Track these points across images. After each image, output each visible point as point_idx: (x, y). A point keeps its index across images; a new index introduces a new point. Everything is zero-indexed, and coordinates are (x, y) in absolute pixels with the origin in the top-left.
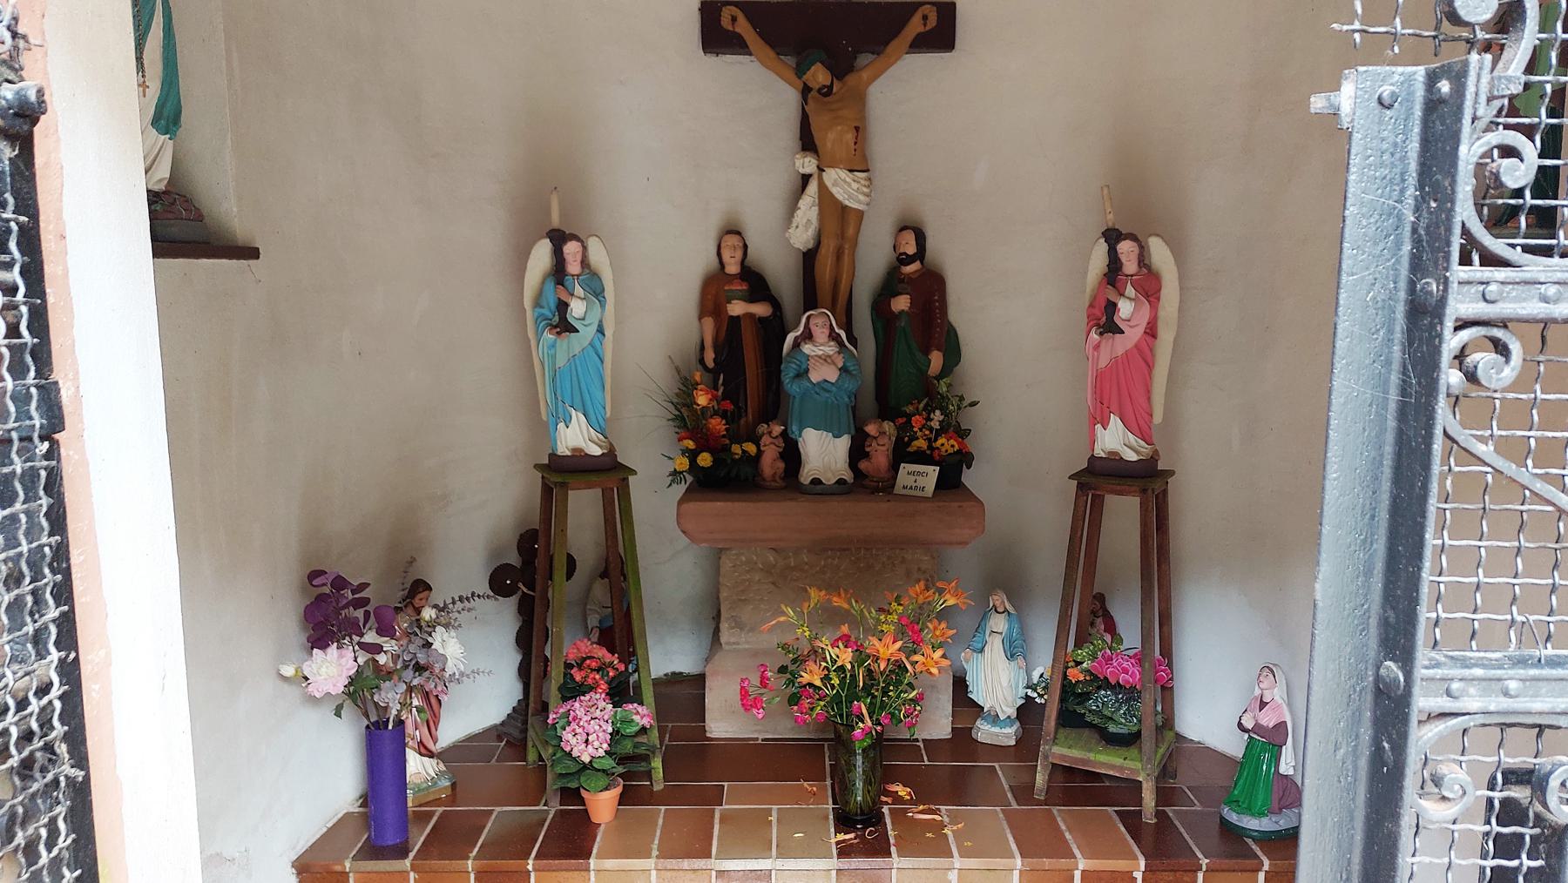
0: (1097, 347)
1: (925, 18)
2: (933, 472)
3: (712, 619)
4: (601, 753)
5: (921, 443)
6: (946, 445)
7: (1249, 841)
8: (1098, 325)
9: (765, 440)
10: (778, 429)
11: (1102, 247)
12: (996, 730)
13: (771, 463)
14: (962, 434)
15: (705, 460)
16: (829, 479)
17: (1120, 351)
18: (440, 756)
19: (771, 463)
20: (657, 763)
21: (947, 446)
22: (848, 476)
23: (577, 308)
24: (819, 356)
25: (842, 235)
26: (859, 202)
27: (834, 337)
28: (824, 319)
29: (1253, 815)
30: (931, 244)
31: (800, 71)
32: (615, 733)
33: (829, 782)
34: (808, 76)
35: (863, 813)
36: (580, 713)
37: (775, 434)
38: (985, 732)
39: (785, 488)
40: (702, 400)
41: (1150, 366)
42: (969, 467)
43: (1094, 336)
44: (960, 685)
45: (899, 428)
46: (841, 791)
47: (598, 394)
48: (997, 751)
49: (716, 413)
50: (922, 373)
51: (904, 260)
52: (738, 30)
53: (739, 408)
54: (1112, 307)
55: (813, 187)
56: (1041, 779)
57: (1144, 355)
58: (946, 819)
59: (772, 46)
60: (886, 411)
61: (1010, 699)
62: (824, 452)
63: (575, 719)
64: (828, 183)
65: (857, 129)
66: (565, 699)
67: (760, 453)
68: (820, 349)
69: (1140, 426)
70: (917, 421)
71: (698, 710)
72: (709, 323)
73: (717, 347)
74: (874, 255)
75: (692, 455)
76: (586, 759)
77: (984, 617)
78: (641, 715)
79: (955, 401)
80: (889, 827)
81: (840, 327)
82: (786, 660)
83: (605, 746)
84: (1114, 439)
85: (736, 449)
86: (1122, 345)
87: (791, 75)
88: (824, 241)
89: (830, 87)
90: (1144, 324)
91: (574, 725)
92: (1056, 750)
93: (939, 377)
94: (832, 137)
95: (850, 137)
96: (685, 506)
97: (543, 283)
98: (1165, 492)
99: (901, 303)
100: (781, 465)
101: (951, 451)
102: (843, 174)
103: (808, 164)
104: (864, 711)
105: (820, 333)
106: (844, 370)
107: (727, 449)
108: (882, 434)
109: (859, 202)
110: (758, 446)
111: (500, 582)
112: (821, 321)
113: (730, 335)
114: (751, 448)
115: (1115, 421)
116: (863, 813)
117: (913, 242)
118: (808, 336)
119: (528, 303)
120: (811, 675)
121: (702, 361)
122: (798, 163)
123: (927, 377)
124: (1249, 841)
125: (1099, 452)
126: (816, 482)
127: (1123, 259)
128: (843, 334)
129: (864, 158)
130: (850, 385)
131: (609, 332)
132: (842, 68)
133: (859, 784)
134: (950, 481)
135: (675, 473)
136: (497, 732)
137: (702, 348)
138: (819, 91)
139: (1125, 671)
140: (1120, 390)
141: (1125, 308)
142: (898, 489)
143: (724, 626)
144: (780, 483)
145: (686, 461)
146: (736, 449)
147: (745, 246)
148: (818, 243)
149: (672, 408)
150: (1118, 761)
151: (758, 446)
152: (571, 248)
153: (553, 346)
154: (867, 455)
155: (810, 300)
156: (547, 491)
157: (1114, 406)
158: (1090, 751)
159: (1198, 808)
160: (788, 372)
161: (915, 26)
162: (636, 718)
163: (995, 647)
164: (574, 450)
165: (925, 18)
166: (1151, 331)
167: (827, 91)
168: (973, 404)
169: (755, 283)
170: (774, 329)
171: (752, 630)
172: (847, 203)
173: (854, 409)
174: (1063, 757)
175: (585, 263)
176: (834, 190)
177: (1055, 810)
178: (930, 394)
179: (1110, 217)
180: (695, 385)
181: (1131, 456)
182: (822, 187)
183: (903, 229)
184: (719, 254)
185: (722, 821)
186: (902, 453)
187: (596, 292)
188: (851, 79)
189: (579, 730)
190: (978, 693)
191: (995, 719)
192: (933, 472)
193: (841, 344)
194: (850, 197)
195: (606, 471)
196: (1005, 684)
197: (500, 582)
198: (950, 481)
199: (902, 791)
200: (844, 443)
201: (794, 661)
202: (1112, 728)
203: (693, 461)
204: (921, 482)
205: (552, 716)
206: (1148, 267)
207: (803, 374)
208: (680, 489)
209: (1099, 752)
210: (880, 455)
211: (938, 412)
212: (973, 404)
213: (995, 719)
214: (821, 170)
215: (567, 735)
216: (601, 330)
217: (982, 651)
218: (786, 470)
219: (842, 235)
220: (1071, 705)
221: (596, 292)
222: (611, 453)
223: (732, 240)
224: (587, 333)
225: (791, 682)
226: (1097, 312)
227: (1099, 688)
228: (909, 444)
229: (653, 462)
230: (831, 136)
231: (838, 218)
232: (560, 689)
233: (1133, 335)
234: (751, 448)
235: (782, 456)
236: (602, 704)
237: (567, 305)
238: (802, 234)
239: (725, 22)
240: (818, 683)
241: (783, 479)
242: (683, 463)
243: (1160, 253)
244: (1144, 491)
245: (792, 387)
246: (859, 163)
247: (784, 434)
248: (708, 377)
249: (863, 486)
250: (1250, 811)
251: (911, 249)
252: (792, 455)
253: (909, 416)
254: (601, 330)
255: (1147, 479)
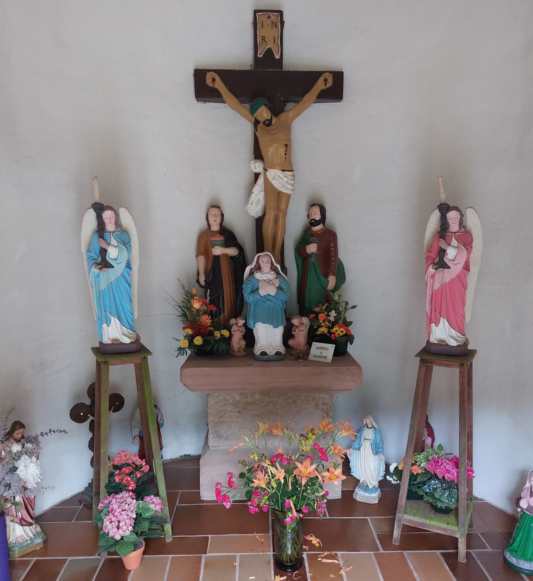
0: (433, 276)
1: (326, 80)
2: (331, 348)
3: (205, 423)
4: (128, 533)
5: (323, 330)
6: (338, 331)
7: (524, 576)
8: (434, 263)
9: (234, 328)
10: (241, 322)
11: (436, 215)
12: (367, 494)
13: (238, 341)
14: (347, 324)
15: (198, 341)
16: (271, 352)
17: (447, 280)
18: (38, 520)
19: (238, 341)
20: (168, 527)
21: (339, 332)
22: (282, 350)
23: (112, 253)
24: (266, 281)
25: (278, 208)
26: (288, 189)
27: (273, 268)
28: (268, 258)
29: (526, 560)
30: (328, 214)
31: (253, 111)
32: (139, 515)
33: (271, 534)
34: (257, 114)
35: (291, 561)
36: (115, 506)
37: (240, 325)
38: (360, 495)
39: (246, 355)
40: (197, 305)
41: (465, 287)
42: (351, 344)
43: (431, 270)
44: (346, 462)
45: (311, 320)
46: (278, 545)
47: (127, 306)
48: (367, 507)
49: (205, 313)
50: (325, 289)
51: (313, 223)
52: (216, 86)
53: (220, 309)
54: (442, 252)
55: (261, 180)
56: (397, 533)
57: (461, 281)
58: (341, 562)
59: (237, 96)
60: (303, 312)
61: (375, 476)
62: (268, 337)
63: (112, 510)
64: (270, 178)
65: (286, 145)
66: (109, 494)
67: (231, 336)
68: (265, 275)
69: (458, 325)
70: (322, 317)
71: (195, 481)
72: (202, 259)
73: (206, 273)
74: (295, 222)
75: (191, 338)
76: (118, 537)
77: (359, 430)
78: (155, 505)
79: (343, 305)
80: (307, 569)
81: (277, 263)
82: (245, 470)
83: (131, 528)
84: (443, 333)
85: (217, 334)
86: (448, 275)
87: (248, 113)
88: (268, 212)
89: (271, 120)
90: (464, 263)
91: (110, 515)
92: (406, 517)
93: (334, 291)
94: (272, 151)
95: (282, 150)
96: (185, 370)
97: (92, 237)
98: (471, 364)
99: (312, 248)
100: (243, 343)
101: (341, 334)
102: (278, 172)
103: (258, 167)
104: (292, 506)
105: (266, 266)
106: (279, 288)
107: (211, 334)
108: (303, 324)
109: (288, 189)
110: (230, 332)
111: (78, 414)
112: (266, 259)
113: (214, 265)
114: (226, 333)
115: (443, 322)
116: (291, 561)
117: (319, 213)
118: (258, 268)
119: (84, 250)
120: (260, 481)
121: (198, 281)
122: (252, 166)
123: (327, 290)
124: (524, 576)
125: (433, 340)
126: (264, 353)
127: (450, 222)
128: (279, 267)
129: (290, 163)
130: (283, 297)
131: (135, 267)
132: (277, 110)
133: (289, 546)
134: (341, 352)
135: (180, 349)
136: (78, 499)
137: (198, 274)
138: (264, 123)
139: (448, 471)
140: (447, 303)
141: (451, 253)
142: (311, 357)
143: (210, 436)
144: (243, 353)
145: (187, 342)
146: (217, 334)
147: (222, 215)
148: (264, 214)
149: (180, 310)
150: (444, 525)
151: (230, 332)
152: (107, 215)
153: (98, 276)
154: (293, 336)
155: (260, 247)
156: (98, 364)
157: (444, 312)
158: (426, 518)
159: (489, 550)
160: (247, 289)
161: (320, 86)
162: (152, 506)
163: (367, 448)
164: (113, 340)
165: (326, 80)
166: (467, 268)
167: (268, 123)
168: (354, 307)
169: (228, 237)
170: (239, 263)
171: (227, 438)
172: (280, 189)
173: (285, 310)
174: (409, 521)
175: (118, 224)
176: (274, 182)
177: (406, 552)
178: (329, 301)
179: (443, 196)
180: (193, 296)
181: (453, 343)
182: (266, 180)
183: (313, 205)
184: (207, 219)
185: (207, 565)
186: (313, 336)
187: (125, 242)
188: (283, 116)
189: (114, 519)
190: (356, 473)
191: (366, 488)
192: (331, 348)
193: (278, 273)
194: (283, 186)
195: (136, 352)
196: (372, 469)
197: (78, 414)
198: (341, 352)
199: (315, 541)
200: (279, 331)
201: (249, 471)
202: (439, 505)
203: (191, 342)
204: (324, 353)
205: (100, 505)
206: (464, 227)
207: (255, 291)
208: (184, 358)
209: (431, 519)
210: (300, 337)
211: (333, 311)
212: (354, 307)
213: (366, 488)
214: (265, 170)
215: (107, 523)
216: (129, 266)
217: (359, 449)
218: (247, 345)
219: (278, 208)
220: (414, 489)
221: (125, 242)
222: (137, 340)
223: (215, 211)
224: (119, 268)
225: (247, 484)
226: (433, 255)
227: (430, 479)
228: (316, 330)
229: (167, 343)
230: (271, 150)
231: (276, 199)
232: (106, 487)
233: (456, 269)
234: (226, 333)
235: (245, 337)
236: (129, 500)
237: (106, 251)
238: (255, 208)
239: (209, 82)
240: (264, 486)
241: (244, 351)
242: (185, 343)
243: (472, 220)
244: (462, 365)
245: (249, 298)
246: (287, 167)
247: (245, 325)
248: (202, 290)
249: (292, 355)
250: (523, 557)
251: (318, 217)
252: (249, 337)
253: (317, 314)
254: (129, 266)
255: (461, 356)
